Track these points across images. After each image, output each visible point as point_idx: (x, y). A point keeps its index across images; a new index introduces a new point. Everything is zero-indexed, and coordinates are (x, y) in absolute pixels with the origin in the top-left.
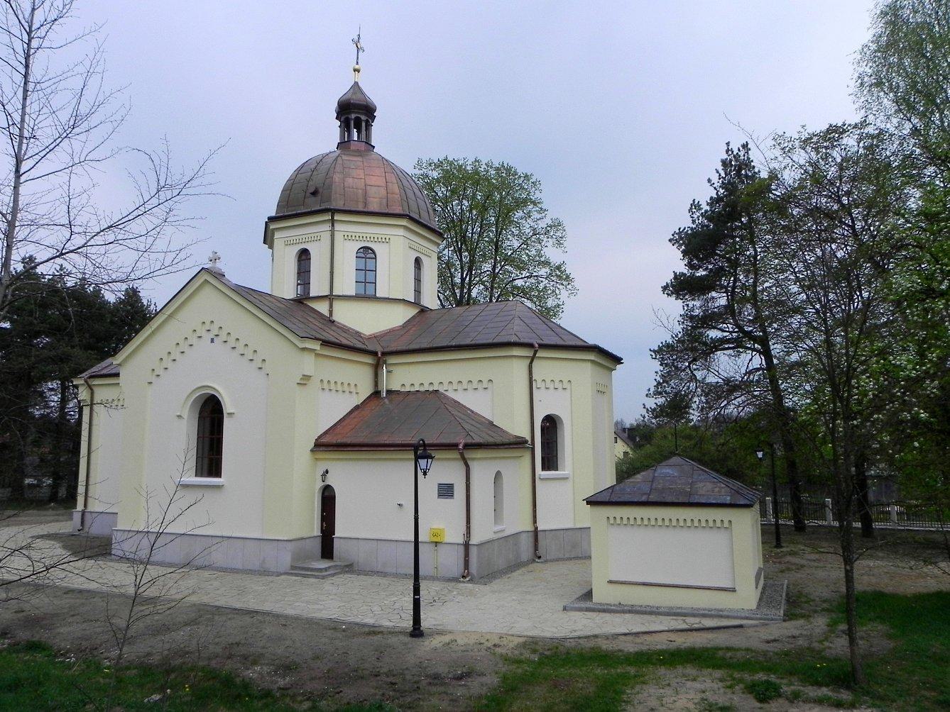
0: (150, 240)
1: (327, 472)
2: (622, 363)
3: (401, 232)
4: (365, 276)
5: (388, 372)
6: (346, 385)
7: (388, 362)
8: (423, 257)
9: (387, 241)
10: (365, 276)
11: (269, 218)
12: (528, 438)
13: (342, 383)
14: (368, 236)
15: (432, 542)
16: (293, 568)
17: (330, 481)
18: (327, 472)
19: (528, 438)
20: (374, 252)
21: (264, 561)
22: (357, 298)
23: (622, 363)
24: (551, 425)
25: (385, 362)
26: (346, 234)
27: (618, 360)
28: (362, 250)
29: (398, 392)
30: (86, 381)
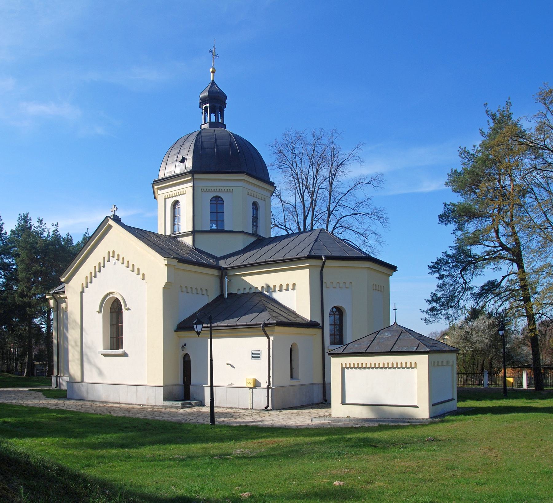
0: (550, 312)
1: (185, 345)
2: (397, 270)
3: (240, 184)
4: (217, 216)
5: (230, 281)
6: (194, 289)
7: (228, 274)
8: (259, 201)
9: (231, 191)
10: (217, 216)
11: (154, 181)
12: (320, 322)
13: (206, 290)
14: (226, 188)
15: (248, 387)
16: (463, 395)
17: (188, 351)
18: (185, 345)
19: (320, 322)
20: (223, 200)
21: (148, 399)
22: (212, 231)
23: (397, 270)
24: (338, 312)
25: (226, 274)
26: (203, 188)
27: (394, 268)
28: (214, 199)
29: (236, 294)
30: (53, 296)
